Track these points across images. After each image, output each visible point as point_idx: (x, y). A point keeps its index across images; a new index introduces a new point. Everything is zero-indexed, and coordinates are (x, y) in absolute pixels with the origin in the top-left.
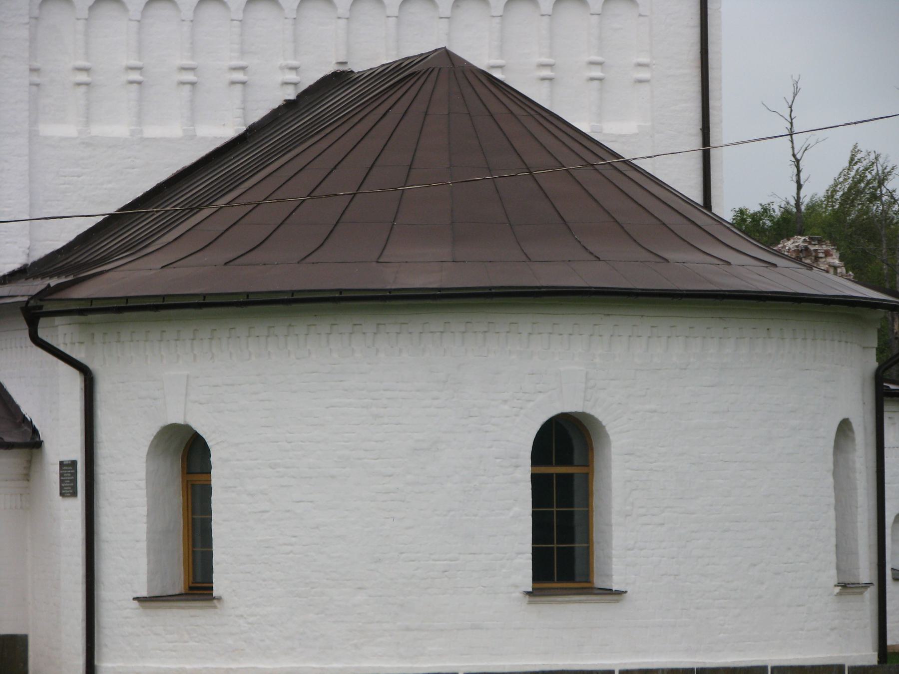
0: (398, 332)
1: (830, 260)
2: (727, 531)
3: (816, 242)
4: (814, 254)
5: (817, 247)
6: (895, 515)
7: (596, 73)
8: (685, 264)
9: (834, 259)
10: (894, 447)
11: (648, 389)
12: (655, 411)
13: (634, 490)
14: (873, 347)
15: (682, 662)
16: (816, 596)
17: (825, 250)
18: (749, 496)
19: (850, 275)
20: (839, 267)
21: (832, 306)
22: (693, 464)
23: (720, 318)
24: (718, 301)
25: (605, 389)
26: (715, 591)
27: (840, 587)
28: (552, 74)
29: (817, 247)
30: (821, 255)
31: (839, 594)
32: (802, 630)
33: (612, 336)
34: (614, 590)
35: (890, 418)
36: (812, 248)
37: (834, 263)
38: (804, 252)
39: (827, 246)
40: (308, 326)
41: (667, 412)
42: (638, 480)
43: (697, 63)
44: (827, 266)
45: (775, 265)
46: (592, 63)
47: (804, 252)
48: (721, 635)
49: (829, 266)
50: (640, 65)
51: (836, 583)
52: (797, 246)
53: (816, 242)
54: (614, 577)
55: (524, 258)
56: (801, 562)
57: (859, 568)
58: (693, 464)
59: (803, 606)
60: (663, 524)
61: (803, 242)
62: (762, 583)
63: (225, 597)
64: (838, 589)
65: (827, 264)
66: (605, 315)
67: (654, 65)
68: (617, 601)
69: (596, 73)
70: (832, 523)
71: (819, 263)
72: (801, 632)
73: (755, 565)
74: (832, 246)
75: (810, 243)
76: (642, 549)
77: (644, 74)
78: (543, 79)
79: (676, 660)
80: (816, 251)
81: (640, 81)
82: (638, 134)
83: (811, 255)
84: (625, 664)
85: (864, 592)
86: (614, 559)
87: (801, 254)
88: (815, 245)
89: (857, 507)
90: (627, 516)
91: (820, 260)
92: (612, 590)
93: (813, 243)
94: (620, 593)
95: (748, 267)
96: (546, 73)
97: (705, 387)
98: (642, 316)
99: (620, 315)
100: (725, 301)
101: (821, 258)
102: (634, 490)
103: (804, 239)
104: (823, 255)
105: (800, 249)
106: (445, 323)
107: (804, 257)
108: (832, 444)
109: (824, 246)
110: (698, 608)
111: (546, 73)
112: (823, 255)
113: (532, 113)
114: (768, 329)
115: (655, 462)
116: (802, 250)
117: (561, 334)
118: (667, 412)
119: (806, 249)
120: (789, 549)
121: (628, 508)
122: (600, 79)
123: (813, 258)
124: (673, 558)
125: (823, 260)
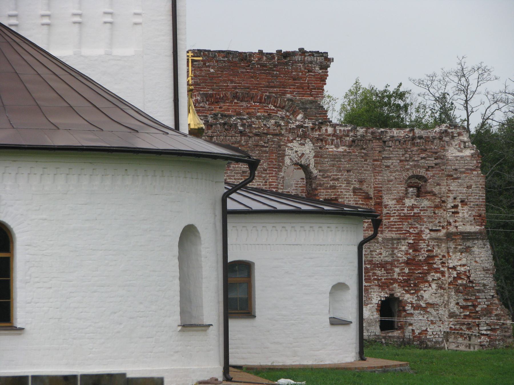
0: (29, 173)
1: (461, 138)
2: (95, 292)
3: (453, 127)
4: (451, 134)
5: (453, 130)
6: (332, 285)
7: (108, 19)
8: (113, 132)
9: (464, 137)
10: (331, 245)
11: (41, 206)
12: (45, 219)
13: (32, 267)
14: (223, 182)
15: (62, 371)
16: (163, 332)
17: (458, 132)
18: (111, 271)
19: (474, 147)
20: (467, 142)
21: (162, 155)
22: (72, 251)
23: (91, 163)
24: (110, 153)
25: (12, 206)
26: (87, 328)
27: (181, 327)
28: (81, 19)
29: (453, 130)
30: (455, 135)
31: (180, 331)
32: (151, 352)
33: (17, 174)
34: (18, 327)
35: (328, 227)
36: (450, 131)
37: (463, 139)
38: (445, 133)
39: (460, 129)
40: (30, 168)
41: (53, 220)
42: (34, 261)
43: (170, 13)
44: (459, 141)
45: (168, 133)
46: (105, 13)
47: (445, 133)
48: (91, 355)
49: (461, 141)
50: (135, 14)
51: (180, 324)
52: (441, 130)
53: (453, 127)
54: (18, 320)
55: (11, 127)
56: (151, 311)
57: (203, 316)
58: (72, 251)
59: (152, 338)
60: (51, 288)
61: (445, 127)
62: (120, 324)
63: (27, 328)
64: (180, 328)
65: (459, 140)
66: (12, 161)
67: (143, 14)
68: (20, 334)
69: (108, 19)
70: (178, 288)
71: (454, 139)
72: (150, 354)
73: (115, 313)
74: (463, 129)
75: (449, 128)
76: (36, 303)
77: (138, 20)
78: (75, 23)
79: (59, 370)
80: (452, 132)
81: (136, 24)
82: (134, 55)
83: (449, 135)
84: (25, 372)
85: (207, 330)
86: (18, 309)
87: (443, 134)
88: (452, 129)
89: (202, 278)
90: (27, 283)
91: (455, 138)
92: (16, 327)
93: (451, 128)
94: (22, 329)
95: (151, 134)
96: (77, 19)
97: (80, 204)
98: (37, 162)
99: (8, 160)
100: (114, 153)
101: (456, 136)
102: (32, 267)
103: (446, 126)
104: (457, 135)
105: (442, 131)
106: (93, 169)
107: (445, 136)
108: (178, 239)
109: (458, 130)
110: (74, 339)
111: (77, 19)
112: (457, 135)
113: (9, 40)
114: (126, 170)
115: (45, 250)
116: (443, 132)
117: (10, 174)
118: (53, 220)
119: (446, 131)
120: (141, 303)
121: (28, 278)
122: (111, 23)
123: (451, 137)
124: (58, 308)
125: (457, 138)
